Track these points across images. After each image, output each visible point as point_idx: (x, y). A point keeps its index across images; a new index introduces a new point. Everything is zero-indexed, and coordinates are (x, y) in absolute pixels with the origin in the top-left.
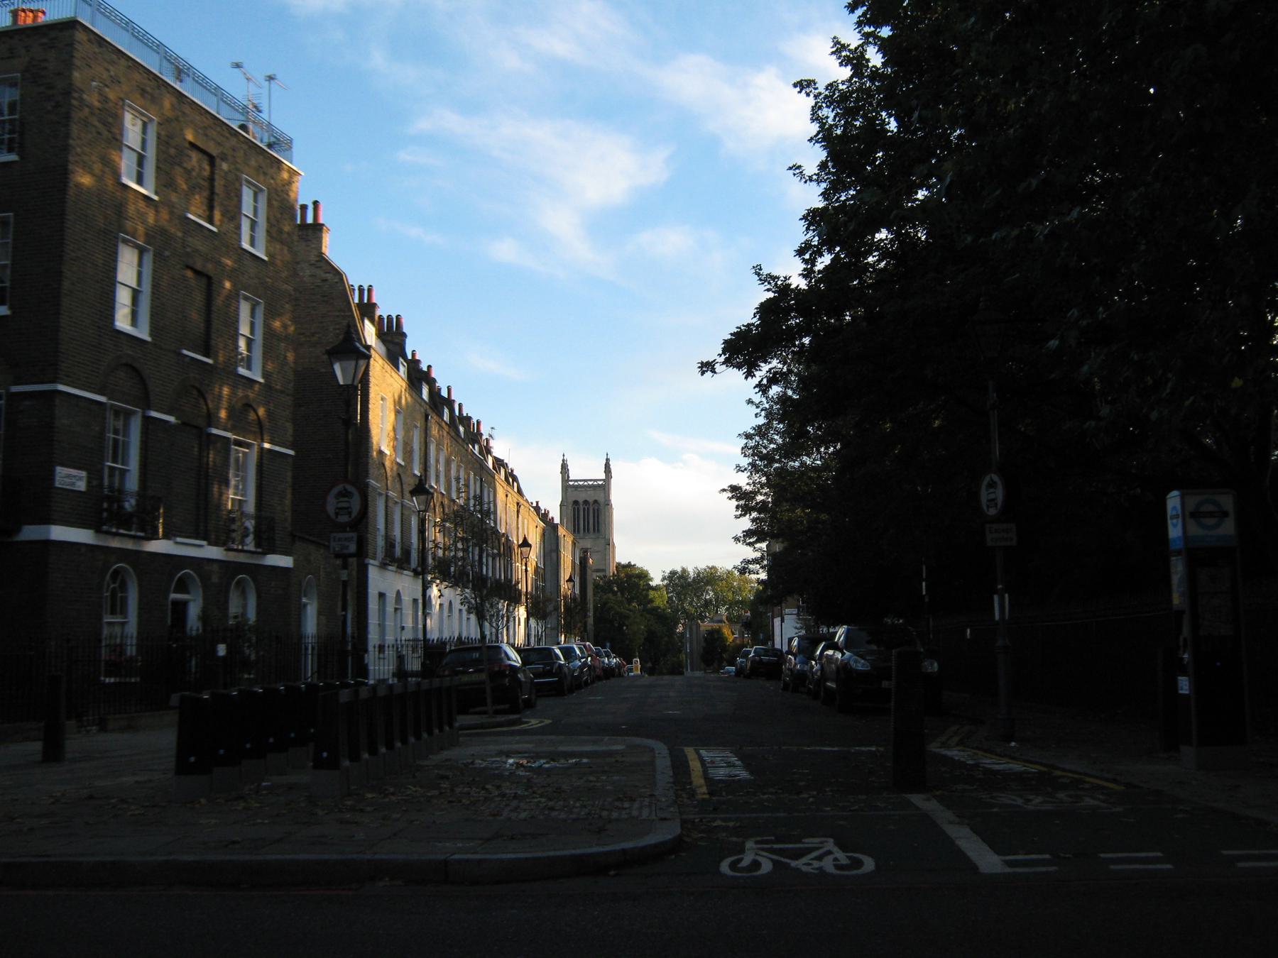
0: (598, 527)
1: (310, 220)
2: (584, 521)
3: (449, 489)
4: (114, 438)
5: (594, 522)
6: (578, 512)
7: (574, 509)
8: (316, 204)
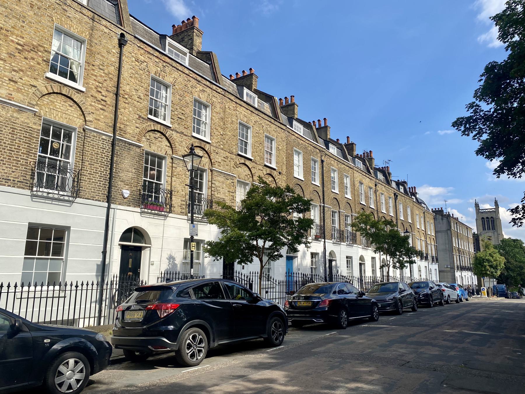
0: (494, 227)
1: (323, 125)
2: (487, 225)
3: (464, 248)
4: (67, 145)
5: (492, 226)
6: (484, 222)
7: (482, 221)
8: (325, 119)
